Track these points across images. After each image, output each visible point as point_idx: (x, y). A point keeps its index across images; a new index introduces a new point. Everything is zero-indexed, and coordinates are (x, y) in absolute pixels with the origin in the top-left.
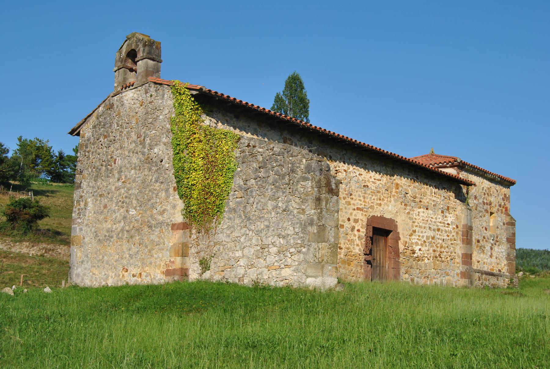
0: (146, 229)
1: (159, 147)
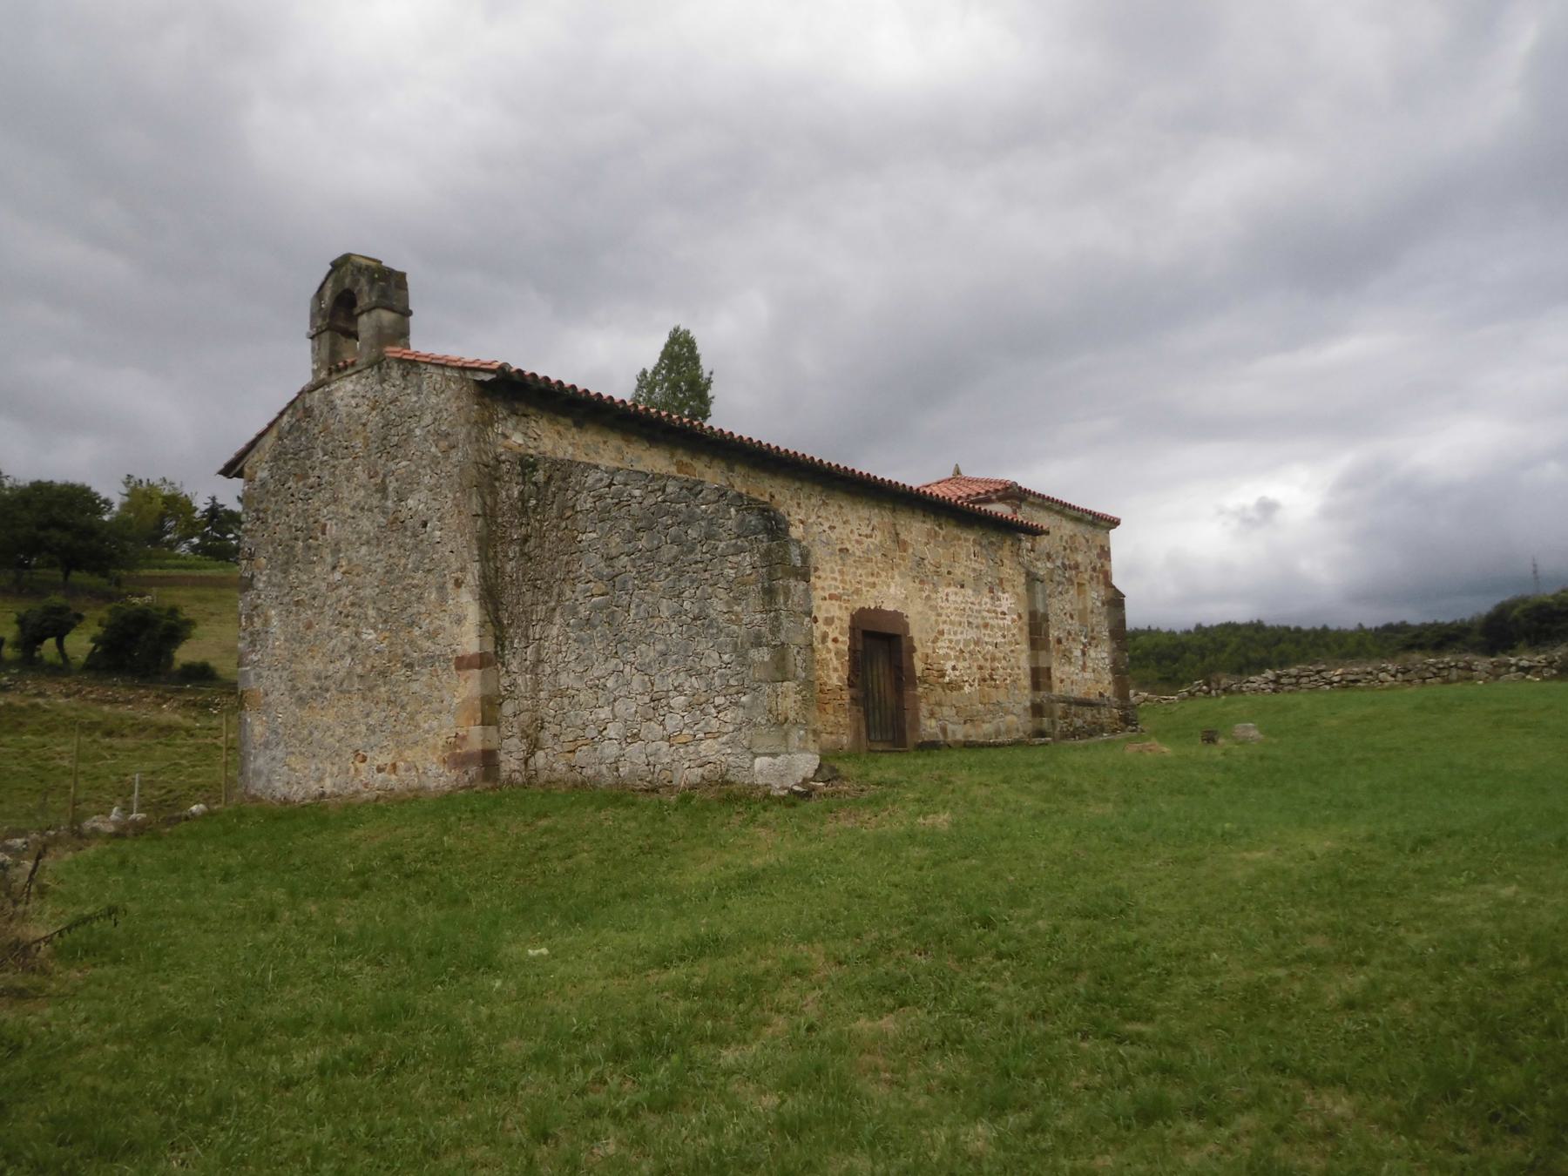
0: (400, 673)
1: (417, 496)
